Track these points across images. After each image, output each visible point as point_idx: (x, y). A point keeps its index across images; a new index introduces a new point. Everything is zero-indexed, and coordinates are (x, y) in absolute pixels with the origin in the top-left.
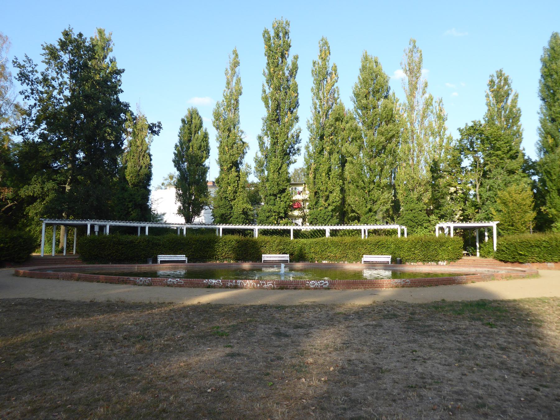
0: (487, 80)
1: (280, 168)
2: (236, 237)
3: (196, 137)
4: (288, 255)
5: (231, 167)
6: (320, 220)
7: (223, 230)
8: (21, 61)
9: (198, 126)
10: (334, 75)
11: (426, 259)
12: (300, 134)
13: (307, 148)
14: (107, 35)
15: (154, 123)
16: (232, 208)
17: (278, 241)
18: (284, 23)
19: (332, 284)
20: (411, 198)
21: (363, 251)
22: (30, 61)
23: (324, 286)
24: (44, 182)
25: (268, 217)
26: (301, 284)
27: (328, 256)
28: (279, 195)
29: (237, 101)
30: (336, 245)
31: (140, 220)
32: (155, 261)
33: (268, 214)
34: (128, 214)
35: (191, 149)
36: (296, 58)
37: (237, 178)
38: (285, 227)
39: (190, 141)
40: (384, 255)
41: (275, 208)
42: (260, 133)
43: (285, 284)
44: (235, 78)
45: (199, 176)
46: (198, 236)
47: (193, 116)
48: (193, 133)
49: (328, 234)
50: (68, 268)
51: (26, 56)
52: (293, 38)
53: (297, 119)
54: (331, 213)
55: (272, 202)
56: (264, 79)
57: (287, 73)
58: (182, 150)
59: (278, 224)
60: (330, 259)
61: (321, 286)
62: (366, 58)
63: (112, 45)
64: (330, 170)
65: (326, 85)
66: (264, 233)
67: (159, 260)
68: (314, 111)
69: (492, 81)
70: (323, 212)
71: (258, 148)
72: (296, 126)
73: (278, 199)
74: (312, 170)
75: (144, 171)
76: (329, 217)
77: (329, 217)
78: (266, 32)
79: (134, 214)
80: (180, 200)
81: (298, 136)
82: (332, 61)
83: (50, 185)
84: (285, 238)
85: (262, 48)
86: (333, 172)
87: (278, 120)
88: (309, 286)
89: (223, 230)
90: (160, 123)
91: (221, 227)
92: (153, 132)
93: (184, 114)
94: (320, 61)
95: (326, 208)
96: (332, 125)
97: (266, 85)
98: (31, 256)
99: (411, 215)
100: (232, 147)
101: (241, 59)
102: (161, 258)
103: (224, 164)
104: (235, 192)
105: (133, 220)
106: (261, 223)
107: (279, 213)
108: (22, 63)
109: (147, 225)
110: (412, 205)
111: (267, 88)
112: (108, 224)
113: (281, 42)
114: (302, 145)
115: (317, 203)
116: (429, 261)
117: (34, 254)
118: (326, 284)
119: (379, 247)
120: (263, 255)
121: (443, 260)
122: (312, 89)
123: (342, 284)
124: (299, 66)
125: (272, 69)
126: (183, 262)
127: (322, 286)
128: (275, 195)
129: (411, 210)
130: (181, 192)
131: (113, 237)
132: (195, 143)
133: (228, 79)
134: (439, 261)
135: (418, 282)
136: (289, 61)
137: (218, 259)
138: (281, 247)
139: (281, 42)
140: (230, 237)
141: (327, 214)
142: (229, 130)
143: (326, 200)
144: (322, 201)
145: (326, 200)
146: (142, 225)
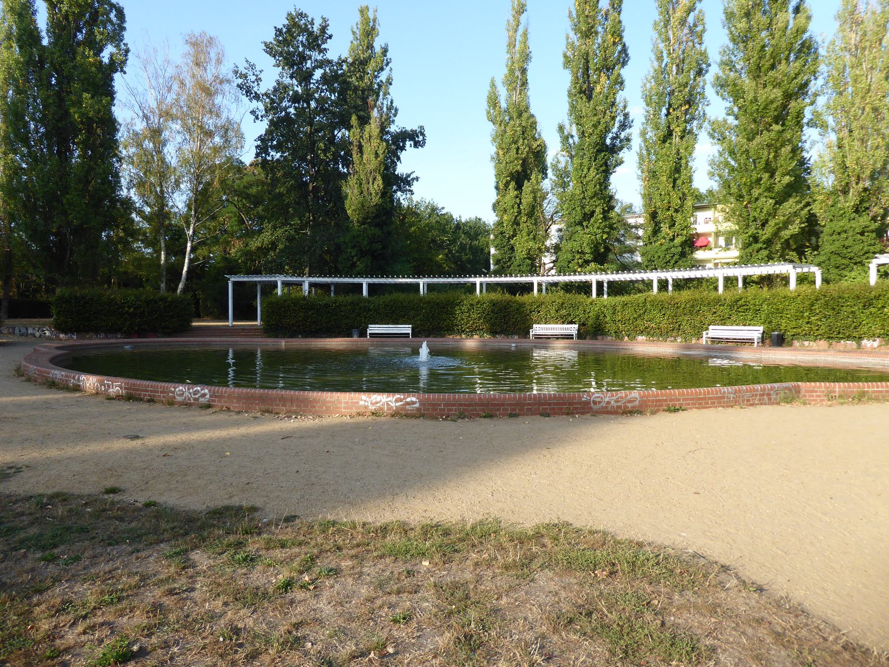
8: (242, 69)
11: (833, 335)
13: (643, 134)
14: (371, 15)
15: (414, 129)
19: (216, 397)
20: (840, 209)
21: (710, 317)
22: (252, 66)
23: (201, 400)
26: (161, 392)
27: (646, 328)
32: (363, 334)
40: (749, 325)
43: (137, 390)
50: (183, 341)
51: (247, 61)
54: (680, 249)
60: (648, 333)
61: (195, 399)
70: (664, 248)
76: (677, 257)
77: (677, 257)
79: (360, 266)
88: (174, 397)
90: (422, 127)
98: (191, 326)
99: (837, 244)
102: (374, 329)
108: (244, 71)
114: (634, 132)
116: (842, 338)
117: (193, 324)
118: (204, 395)
119: (740, 310)
120: (535, 326)
121: (873, 336)
122: (656, 24)
123: (235, 398)
126: (406, 335)
127: (197, 399)
129: (839, 234)
131: (369, 302)
134: (860, 338)
135: (444, 405)
137: (463, 331)
144: (665, 228)
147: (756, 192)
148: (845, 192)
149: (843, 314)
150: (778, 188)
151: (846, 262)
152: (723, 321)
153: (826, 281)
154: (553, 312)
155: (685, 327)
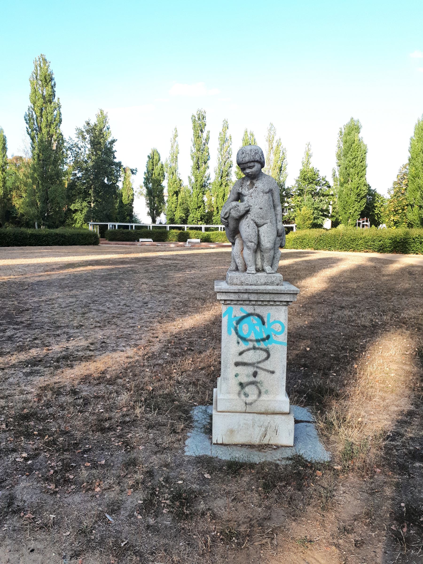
0: (338, 131)
3: (156, 168)
7: (118, 225)
9: (158, 160)
16: (174, 215)
24: (82, 203)
29: (177, 157)
31: (130, 222)
32: (138, 241)
34: (125, 219)
35: (153, 176)
36: (209, 132)
38: (201, 226)
39: (153, 170)
41: (196, 216)
44: (176, 144)
45: (159, 192)
46: (157, 230)
47: (155, 154)
48: (155, 165)
49: (203, 229)
52: (208, 121)
53: (208, 167)
56: (191, 144)
57: (204, 141)
58: (148, 175)
64: (224, 195)
65: (226, 145)
66: (192, 228)
67: (140, 241)
68: (218, 162)
69: (341, 132)
72: (208, 172)
75: (131, 197)
80: (148, 207)
82: (229, 133)
83: (85, 204)
84: (199, 232)
86: (226, 197)
89: (118, 225)
92: (133, 173)
93: (149, 152)
96: (226, 171)
97: (193, 147)
100: (174, 183)
102: (141, 240)
103: (170, 192)
104: (176, 207)
105: (126, 222)
109: (134, 225)
111: (193, 149)
112: (117, 224)
124: (210, 137)
128: (196, 209)
130: (148, 202)
132: (156, 171)
133: (172, 144)
136: (205, 135)
138: (196, 236)
142: (173, 173)
146: (132, 224)
154: (193, 236)
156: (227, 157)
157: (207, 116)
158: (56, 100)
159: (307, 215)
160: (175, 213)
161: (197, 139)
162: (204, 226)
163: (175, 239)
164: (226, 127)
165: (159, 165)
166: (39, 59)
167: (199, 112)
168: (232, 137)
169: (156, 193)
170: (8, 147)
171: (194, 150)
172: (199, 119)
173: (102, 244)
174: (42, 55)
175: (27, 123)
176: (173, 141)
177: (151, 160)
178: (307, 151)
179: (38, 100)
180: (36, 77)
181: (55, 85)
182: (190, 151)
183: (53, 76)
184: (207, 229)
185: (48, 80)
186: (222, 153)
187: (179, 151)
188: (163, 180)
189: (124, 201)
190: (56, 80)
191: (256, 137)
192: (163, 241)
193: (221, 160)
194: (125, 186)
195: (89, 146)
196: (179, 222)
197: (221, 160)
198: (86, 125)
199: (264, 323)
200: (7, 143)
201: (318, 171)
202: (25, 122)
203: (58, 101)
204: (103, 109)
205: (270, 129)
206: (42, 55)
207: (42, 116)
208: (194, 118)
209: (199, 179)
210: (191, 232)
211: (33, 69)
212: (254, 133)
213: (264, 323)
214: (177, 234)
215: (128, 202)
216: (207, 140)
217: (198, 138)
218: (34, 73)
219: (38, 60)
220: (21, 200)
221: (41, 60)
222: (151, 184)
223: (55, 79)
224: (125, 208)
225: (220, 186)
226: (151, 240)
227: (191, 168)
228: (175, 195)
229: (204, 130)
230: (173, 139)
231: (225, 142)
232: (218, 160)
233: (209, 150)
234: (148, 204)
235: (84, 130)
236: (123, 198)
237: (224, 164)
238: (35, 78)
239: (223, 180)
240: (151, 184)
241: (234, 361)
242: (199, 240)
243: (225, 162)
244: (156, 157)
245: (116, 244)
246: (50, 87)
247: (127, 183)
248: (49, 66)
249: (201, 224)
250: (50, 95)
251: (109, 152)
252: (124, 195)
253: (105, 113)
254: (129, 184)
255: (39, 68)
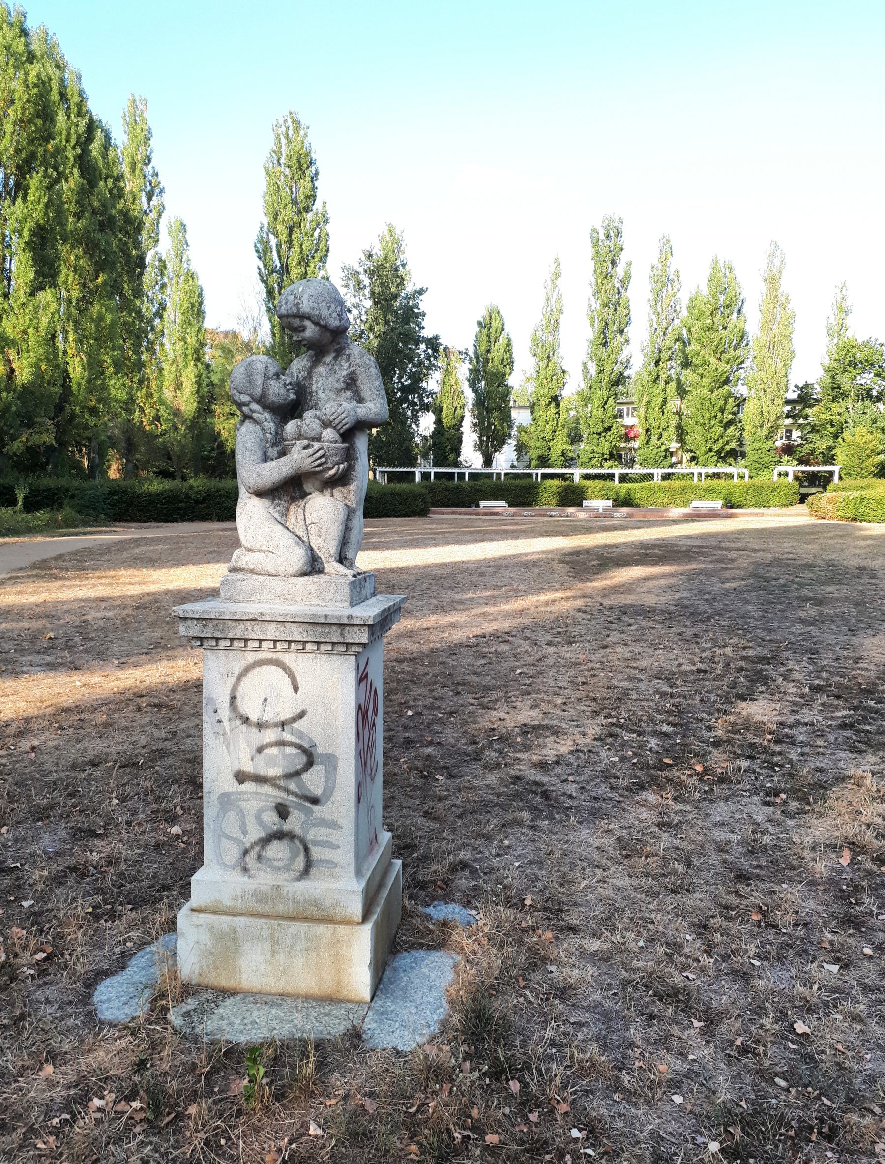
1: (606, 403)
2: (556, 482)
4: (611, 501)
5: (550, 402)
6: (651, 461)
9: (500, 328)
10: (676, 282)
12: (631, 360)
17: (601, 486)
18: (617, 220)
25: (590, 459)
28: (603, 434)
30: (664, 490)
32: (478, 506)
33: (591, 456)
34: (446, 458)
35: (490, 364)
36: (629, 264)
37: (557, 416)
38: (610, 471)
39: (488, 351)
42: (584, 357)
47: (493, 317)
48: (492, 340)
52: (626, 240)
55: (596, 441)
56: (589, 291)
59: (602, 466)
62: (715, 268)
63: (403, 246)
64: (665, 402)
66: (586, 477)
68: (649, 329)
70: (654, 452)
71: (580, 377)
73: (602, 438)
74: (644, 403)
78: (594, 230)
81: (628, 362)
82: (674, 263)
84: (608, 483)
85: (588, 250)
87: (605, 345)
91: (540, 471)
93: (480, 314)
94: (660, 265)
95: (659, 447)
96: (670, 349)
97: (592, 298)
99: (757, 456)
101: (563, 269)
102: (483, 503)
105: (449, 466)
106: (583, 465)
107: (603, 455)
110: (759, 445)
113: (611, 244)
115: (647, 442)
125: (599, 281)
128: (600, 434)
132: (496, 354)
136: (620, 270)
138: (604, 493)
139: (611, 244)
140: (550, 482)
141: (660, 454)
143: (659, 438)
144: (654, 439)
145: (659, 438)
147: (713, 422)
148: (761, 427)
149: (762, 495)
150: (725, 421)
151: (760, 466)
152: (700, 498)
153: (751, 477)
154: (596, 493)
155: (678, 502)
156: (671, 317)
157: (625, 229)
158: (318, 206)
159: (870, 445)
160: (551, 444)
161: (605, 281)
162: (617, 471)
163: (553, 502)
164: (667, 251)
165: (502, 340)
166: (286, 121)
167: (607, 222)
168: (681, 274)
169: (495, 402)
170: (206, 310)
171: (597, 305)
172: (608, 236)
173: (435, 513)
174: (291, 113)
175: (260, 258)
176: (549, 287)
177: (485, 331)
178: (839, 300)
179: (285, 208)
180: (278, 161)
181: (317, 174)
182: (586, 308)
183: (314, 156)
184: (623, 478)
185: (305, 166)
186: (659, 310)
187: (563, 308)
188: (510, 374)
189: (445, 421)
190: (319, 164)
191: (737, 272)
192: (529, 505)
193: (656, 326)
194: (447, 388)
195: (368, 304)
196: (559, 463)
197: (656, 326)
198: (363, 258)
199: (296, 689)
200: (205, 302)
201: (882, 345)
202: (256, 255)
203: (324, 207)
204: (393, 224)
205: (772, 255)
206: (291, 113)
207: (290, 242)
208: (595, 235)
209: (607, 368)
210: (588, 483)
211: (271, 144)
212: (734, 265)
213: (296, 689)
214: (560, 490)
215: (454, 422)
216: (625, 281)
217: (606, 278)
218: (274, 152)
219: (281, 122)
220: (232, 421)
221: (289, 123)
222: (483, 383)
223: (317, 162)
224: (447, 435)
225: (655, 381)
226: (503, 503)
227: (587, 343)
228: (553, 404)
229: (618, 261)
230: (549, 283)
231: (665, 285)
232: (648, 325)
233: (630, 303)
234: (475, 425)
235: (361, 270)
236: (444, 414)
237: (664, 334)
238: (276, 162)
239: (659, 368)
240: (483, 383)
241: (236, 768)
242: (610, 503)
243: (667, 329)
244: (495, 324)
245: (453, 513)
246: (308, 179)
247: (453, 382)
248: (306, 135)
249: (611, 467)
250: (307, 197)
251: (411, 315)
252: (445, 408)
253: (398, 231)
254: (457, 383)
255: (284, 141)
